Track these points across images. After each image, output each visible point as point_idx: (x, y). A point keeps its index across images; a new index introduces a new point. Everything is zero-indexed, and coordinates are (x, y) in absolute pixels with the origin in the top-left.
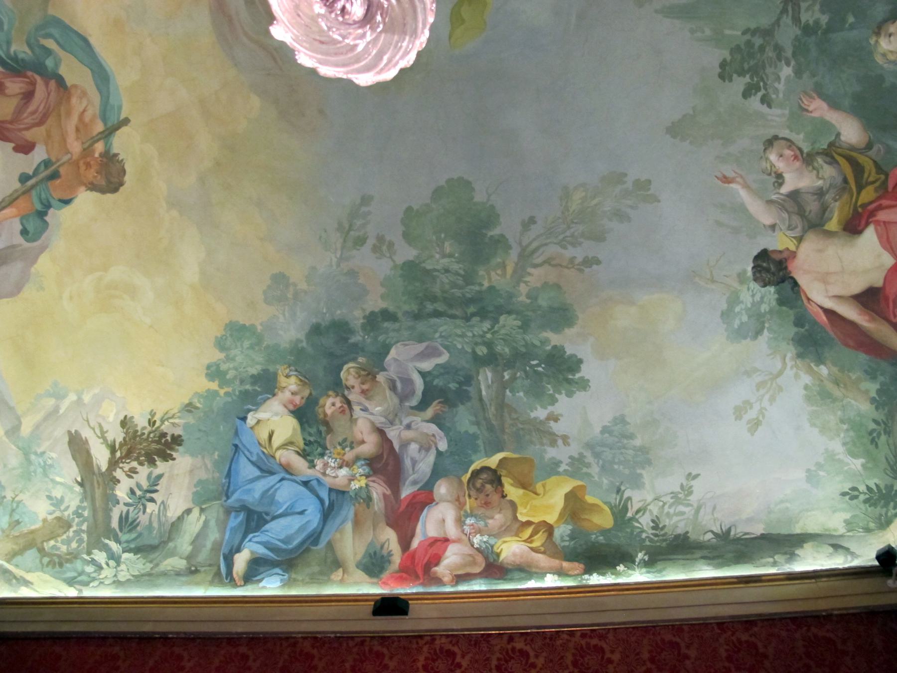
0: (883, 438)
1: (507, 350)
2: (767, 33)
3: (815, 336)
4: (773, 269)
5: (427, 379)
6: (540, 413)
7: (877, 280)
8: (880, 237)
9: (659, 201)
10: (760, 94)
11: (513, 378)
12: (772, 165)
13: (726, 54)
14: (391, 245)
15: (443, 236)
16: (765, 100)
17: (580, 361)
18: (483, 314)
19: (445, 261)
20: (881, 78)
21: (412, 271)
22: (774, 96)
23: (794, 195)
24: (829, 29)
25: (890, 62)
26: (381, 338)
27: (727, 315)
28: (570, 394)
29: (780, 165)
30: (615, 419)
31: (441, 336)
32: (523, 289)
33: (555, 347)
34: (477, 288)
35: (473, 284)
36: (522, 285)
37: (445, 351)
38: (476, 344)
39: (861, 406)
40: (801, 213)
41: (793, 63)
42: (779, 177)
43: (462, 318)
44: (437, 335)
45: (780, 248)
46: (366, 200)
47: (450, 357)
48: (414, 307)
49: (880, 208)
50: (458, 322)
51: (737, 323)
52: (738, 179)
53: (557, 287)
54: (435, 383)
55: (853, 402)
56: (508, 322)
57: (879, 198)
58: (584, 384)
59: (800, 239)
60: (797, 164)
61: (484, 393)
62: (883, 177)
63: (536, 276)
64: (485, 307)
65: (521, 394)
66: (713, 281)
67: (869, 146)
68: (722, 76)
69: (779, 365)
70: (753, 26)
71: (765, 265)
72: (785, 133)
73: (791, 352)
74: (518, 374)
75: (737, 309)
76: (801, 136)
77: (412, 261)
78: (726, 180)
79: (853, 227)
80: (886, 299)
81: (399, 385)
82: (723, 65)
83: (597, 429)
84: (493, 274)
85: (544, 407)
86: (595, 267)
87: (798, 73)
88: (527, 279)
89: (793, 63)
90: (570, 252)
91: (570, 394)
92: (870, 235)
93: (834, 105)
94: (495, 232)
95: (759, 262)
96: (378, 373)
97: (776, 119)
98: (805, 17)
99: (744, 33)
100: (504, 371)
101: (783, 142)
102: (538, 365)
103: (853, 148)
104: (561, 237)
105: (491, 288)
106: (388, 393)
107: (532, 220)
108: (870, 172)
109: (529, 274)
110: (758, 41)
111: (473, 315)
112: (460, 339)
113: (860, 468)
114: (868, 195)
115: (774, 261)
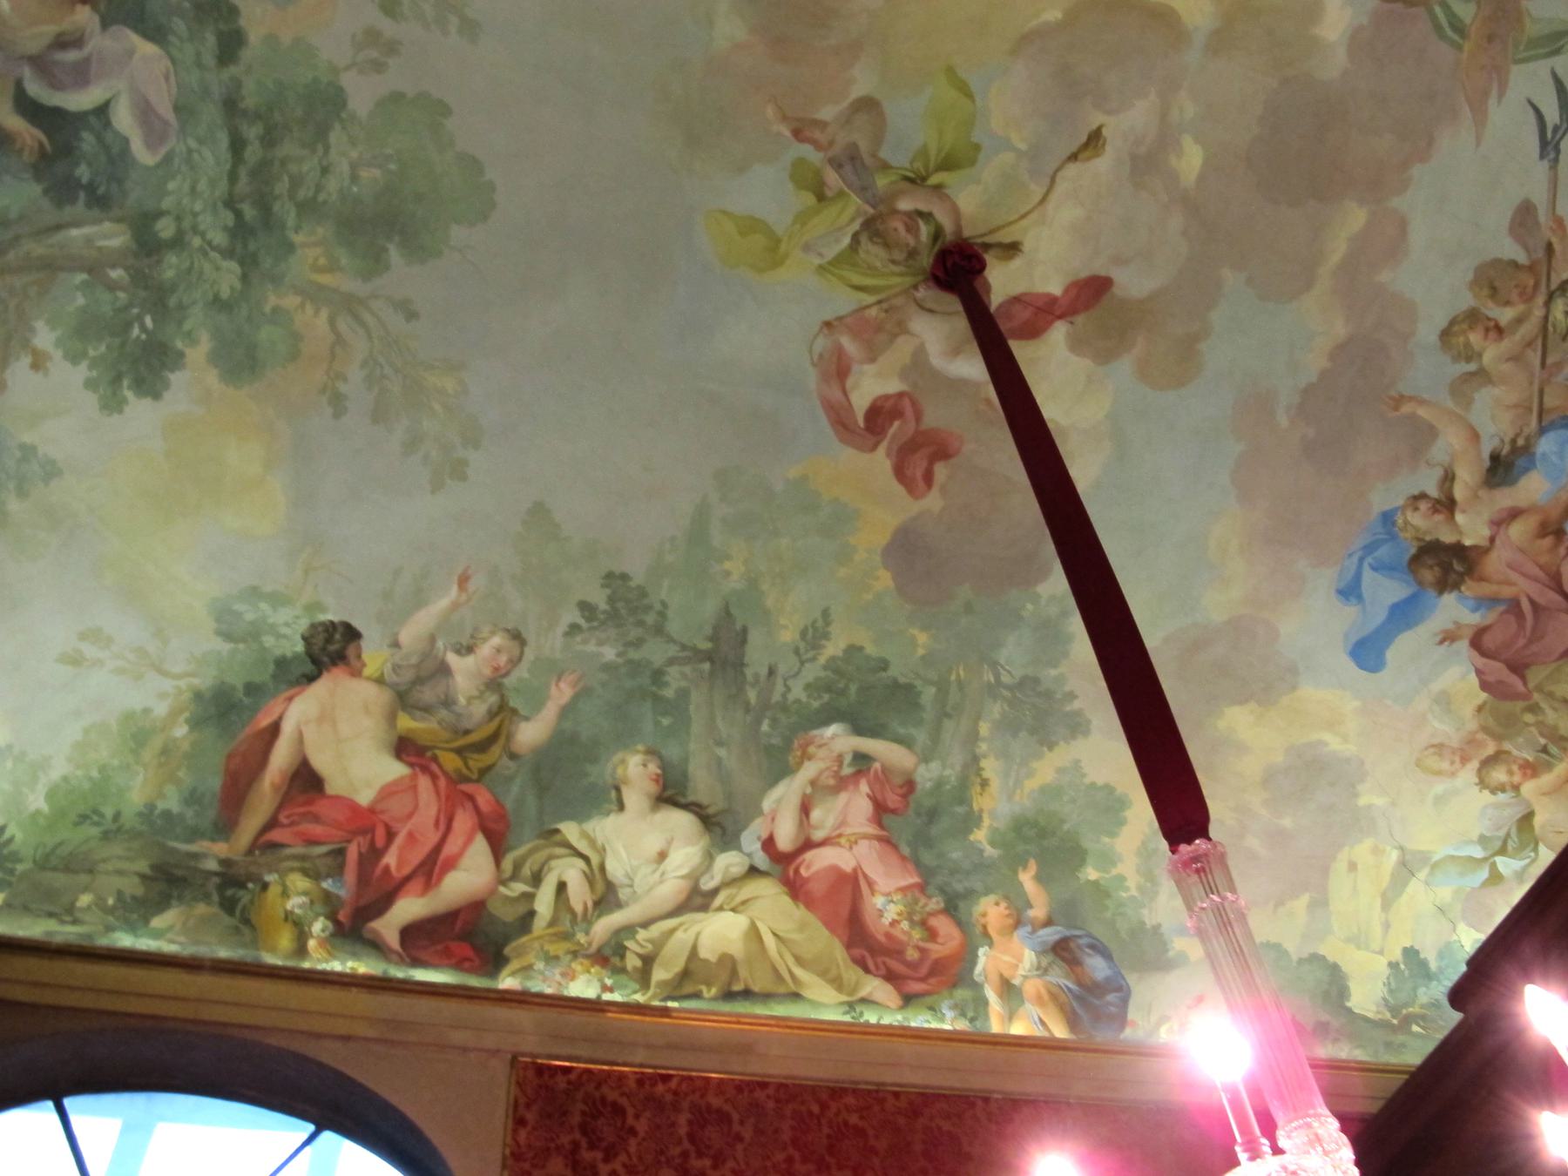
0: (94, 831)
1: (170, 274)
2: (659, 630)
3: (234, 717)
4: (332, 648)
5: (92, 120)
6: (44, 337)
7: (334, 786)
8: (395, 783)
9: (433, 492)
10: (582, 622)
11: (112, 287)
12: (485, 640)
13: (638, 579)
14: (378, 67)
15: (392, 167)
16: (574, 629)
17: (157, 396)
18: (240, 230)
19: (345, 168)
20: (594, 760)
21: (325, 105)
22: (578, 639)
23: (444, 670)
24: (657, 699)
25: (614, 769)
26: (179, 25)
27: (254, 593)
28: (90, 384)
29: (485, 650)
30: (53, 462)
31: (190, 151)
32: (291, 301)
33: (181, 355)
34: (291, 221)
35: (299, 215)
36: (298, 300)
37: (158, 158)
38: (178, 219)
39: (137, 790)
40: (419, 681)
41: (620, 660)
42: (470, 650)
43: (231, 194)
44: (192, 143)
45: (365, 656)
46: (470, 29)
47: (147, 168)
48: (250, 101)
49: (434, 778)
50: (223, 185)
51: (238, 607)
52: (464, 597)
53: (294, 356)
54: (85, 135)
55: (140, 778)
56: (227, 277)
57: (445, 773)
58: (113, 404)
59: (380, 681)
60: (487, 672)
61: (74, 232)
62: (475, 776)
63: (315, 323)
64: (253, 234)
65: (80, 301)
66: (306, 572)
67: (513, 756)
68: (610, 576)
69: (177, 669)
70: (670, 613)
71: (338, 636)
72: (529, 654)
73: (205, 681)
74: (122, 295)
75: (263, 606)
76: (526, 675)
77: (344, 104)
78: (463, 581)
79: (404, 748)
80: (309, 802)
81: (71, 56)
82: (624, 577)
83: (27, 438)
84: (318, 250)
85: (59, 343)
86: (329, 411)
87: (608, 668)
88: (309, 310)
89: (620, 660)
90: (356, 374)
91: (90, 384)
92: (396, 770)
93: (565, 712)
94: (394, 254)
95: (340, 629)
96: (95, 8)
97: (548, 643)
98: (673, 671)
99: (664, 604)
100: (126, 269)
101: (516, 652)
102: (143, 328)
103: (509, 737)
104: (381, 359)
105: (290, 248)
106: (50, 30)
107: (412, 316)
108: (478, 761)
109: (317, 312)
110: (650, 619)
111: (238, 215)
112: (186, 187)
113: (32, 808)
114: (451, 761)
115: (344, 648)
